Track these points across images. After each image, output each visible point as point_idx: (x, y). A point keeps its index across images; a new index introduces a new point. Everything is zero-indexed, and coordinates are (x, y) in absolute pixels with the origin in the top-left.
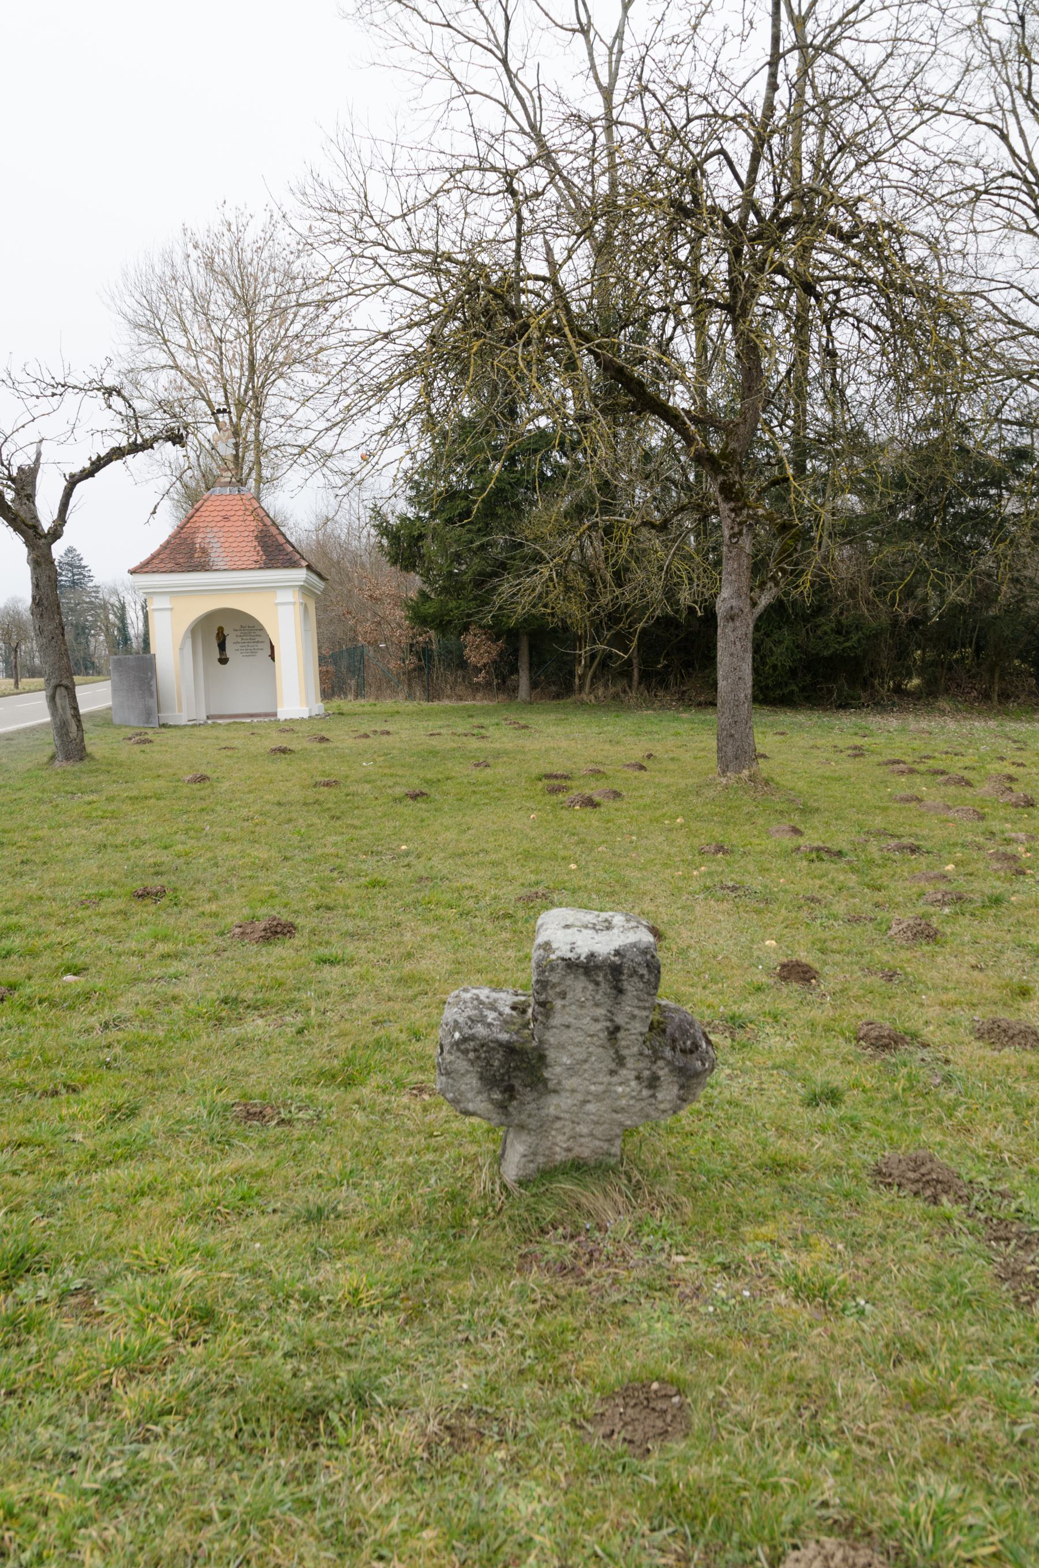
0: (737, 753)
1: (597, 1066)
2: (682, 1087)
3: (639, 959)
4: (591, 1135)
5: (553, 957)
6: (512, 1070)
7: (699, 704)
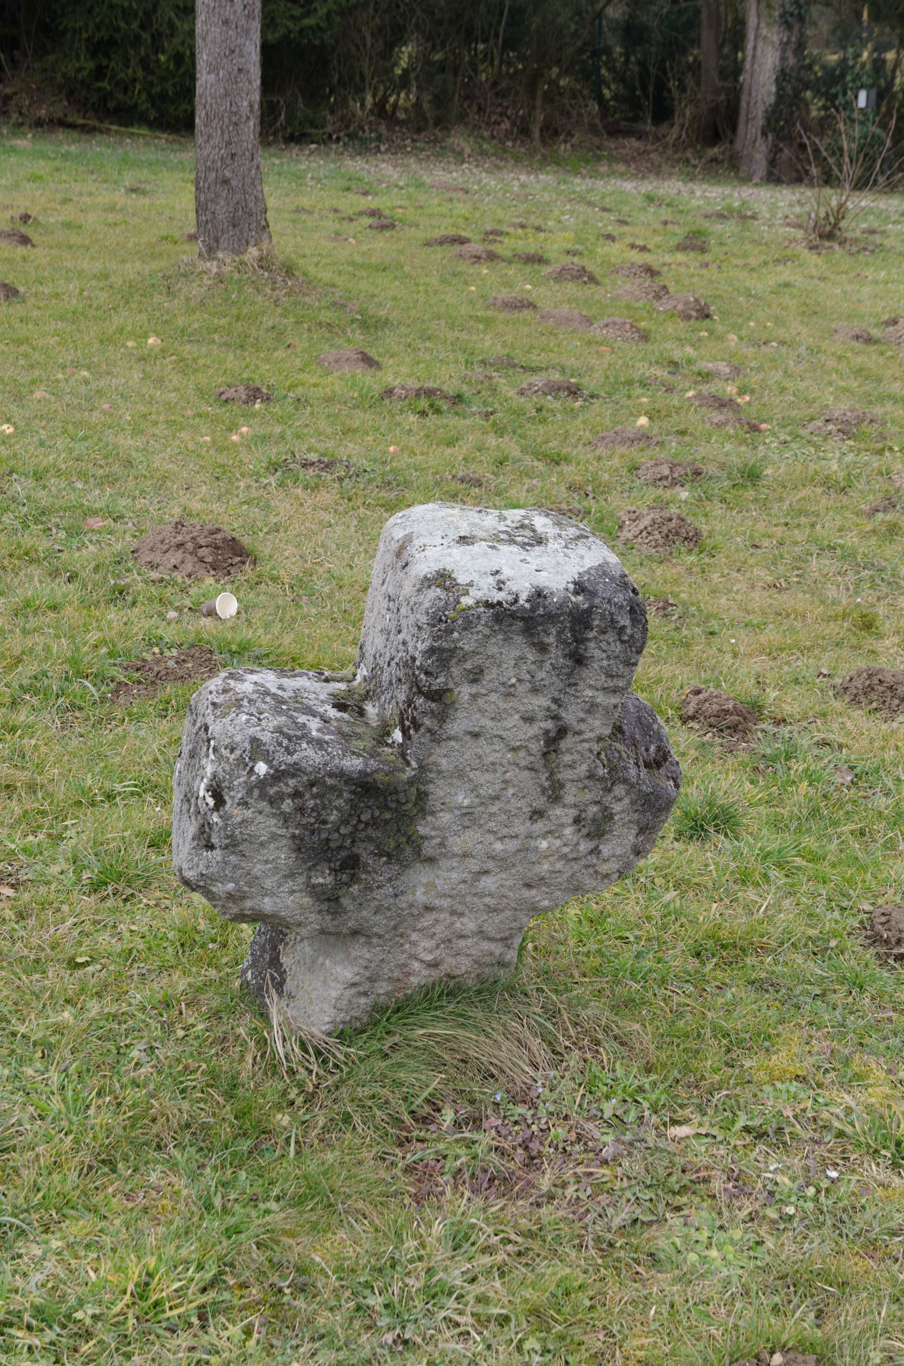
0: (228, 219)
1: (515, 804)
2: (642, 830)
3: (619, 598)
4: (481, 933)
5: (467, 601)
6: (357, 826)
7: (39, 123)
